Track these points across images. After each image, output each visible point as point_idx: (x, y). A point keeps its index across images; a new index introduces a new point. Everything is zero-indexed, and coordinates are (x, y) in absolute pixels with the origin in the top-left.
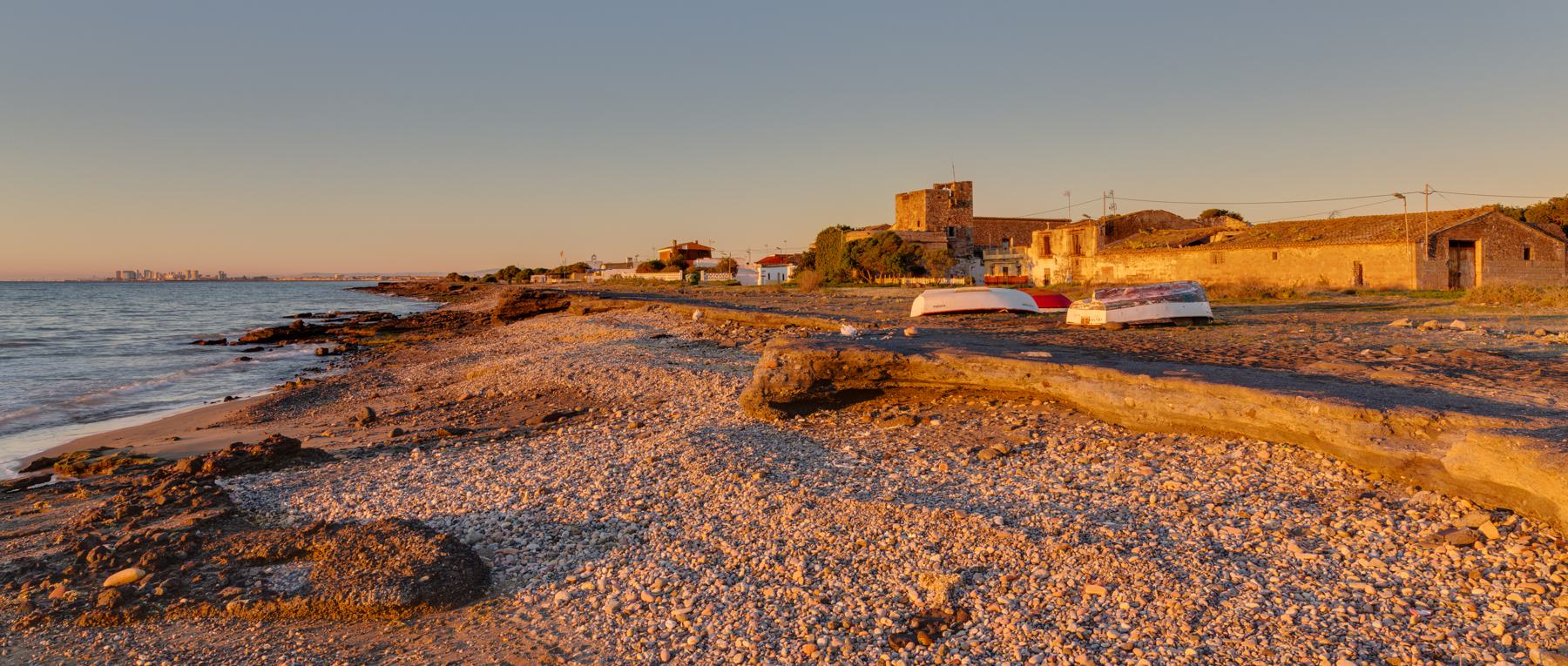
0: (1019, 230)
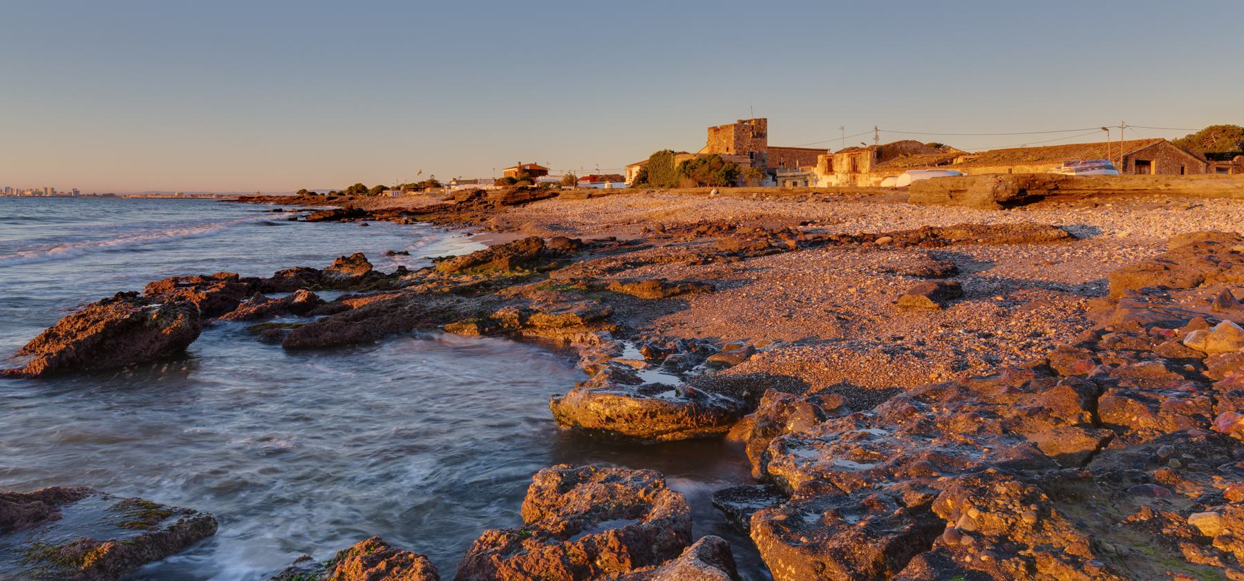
0: (809, 156)
